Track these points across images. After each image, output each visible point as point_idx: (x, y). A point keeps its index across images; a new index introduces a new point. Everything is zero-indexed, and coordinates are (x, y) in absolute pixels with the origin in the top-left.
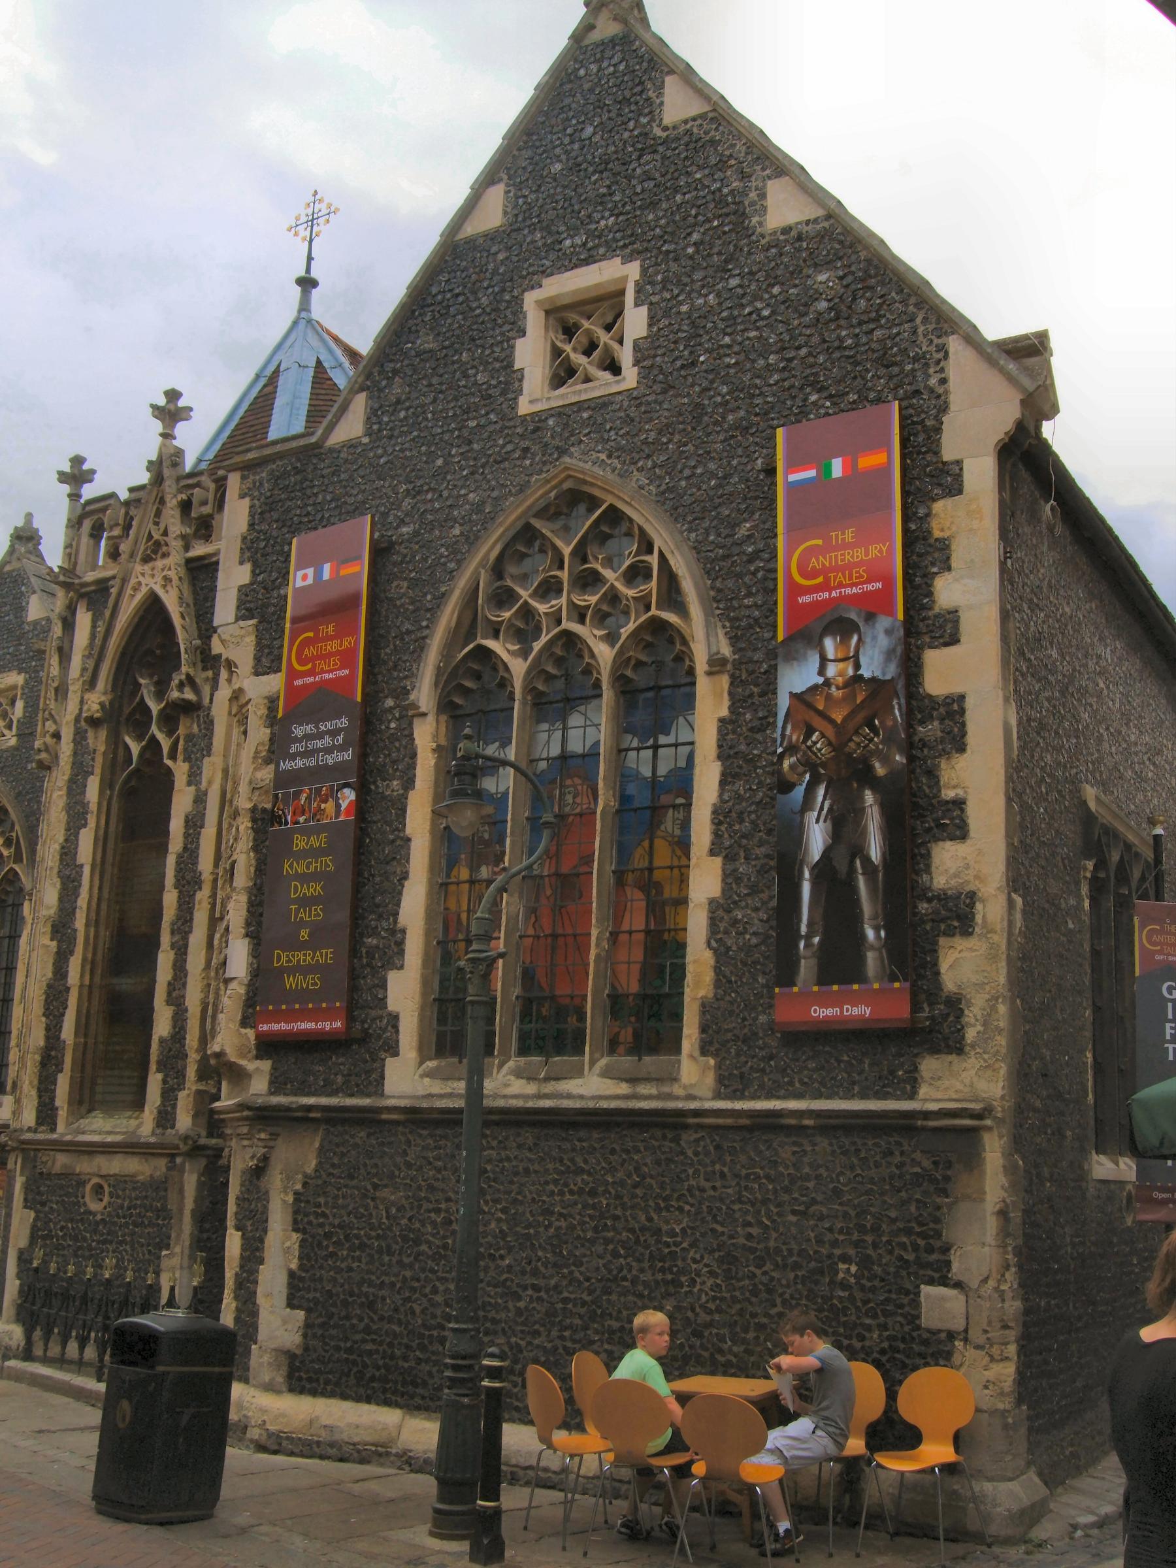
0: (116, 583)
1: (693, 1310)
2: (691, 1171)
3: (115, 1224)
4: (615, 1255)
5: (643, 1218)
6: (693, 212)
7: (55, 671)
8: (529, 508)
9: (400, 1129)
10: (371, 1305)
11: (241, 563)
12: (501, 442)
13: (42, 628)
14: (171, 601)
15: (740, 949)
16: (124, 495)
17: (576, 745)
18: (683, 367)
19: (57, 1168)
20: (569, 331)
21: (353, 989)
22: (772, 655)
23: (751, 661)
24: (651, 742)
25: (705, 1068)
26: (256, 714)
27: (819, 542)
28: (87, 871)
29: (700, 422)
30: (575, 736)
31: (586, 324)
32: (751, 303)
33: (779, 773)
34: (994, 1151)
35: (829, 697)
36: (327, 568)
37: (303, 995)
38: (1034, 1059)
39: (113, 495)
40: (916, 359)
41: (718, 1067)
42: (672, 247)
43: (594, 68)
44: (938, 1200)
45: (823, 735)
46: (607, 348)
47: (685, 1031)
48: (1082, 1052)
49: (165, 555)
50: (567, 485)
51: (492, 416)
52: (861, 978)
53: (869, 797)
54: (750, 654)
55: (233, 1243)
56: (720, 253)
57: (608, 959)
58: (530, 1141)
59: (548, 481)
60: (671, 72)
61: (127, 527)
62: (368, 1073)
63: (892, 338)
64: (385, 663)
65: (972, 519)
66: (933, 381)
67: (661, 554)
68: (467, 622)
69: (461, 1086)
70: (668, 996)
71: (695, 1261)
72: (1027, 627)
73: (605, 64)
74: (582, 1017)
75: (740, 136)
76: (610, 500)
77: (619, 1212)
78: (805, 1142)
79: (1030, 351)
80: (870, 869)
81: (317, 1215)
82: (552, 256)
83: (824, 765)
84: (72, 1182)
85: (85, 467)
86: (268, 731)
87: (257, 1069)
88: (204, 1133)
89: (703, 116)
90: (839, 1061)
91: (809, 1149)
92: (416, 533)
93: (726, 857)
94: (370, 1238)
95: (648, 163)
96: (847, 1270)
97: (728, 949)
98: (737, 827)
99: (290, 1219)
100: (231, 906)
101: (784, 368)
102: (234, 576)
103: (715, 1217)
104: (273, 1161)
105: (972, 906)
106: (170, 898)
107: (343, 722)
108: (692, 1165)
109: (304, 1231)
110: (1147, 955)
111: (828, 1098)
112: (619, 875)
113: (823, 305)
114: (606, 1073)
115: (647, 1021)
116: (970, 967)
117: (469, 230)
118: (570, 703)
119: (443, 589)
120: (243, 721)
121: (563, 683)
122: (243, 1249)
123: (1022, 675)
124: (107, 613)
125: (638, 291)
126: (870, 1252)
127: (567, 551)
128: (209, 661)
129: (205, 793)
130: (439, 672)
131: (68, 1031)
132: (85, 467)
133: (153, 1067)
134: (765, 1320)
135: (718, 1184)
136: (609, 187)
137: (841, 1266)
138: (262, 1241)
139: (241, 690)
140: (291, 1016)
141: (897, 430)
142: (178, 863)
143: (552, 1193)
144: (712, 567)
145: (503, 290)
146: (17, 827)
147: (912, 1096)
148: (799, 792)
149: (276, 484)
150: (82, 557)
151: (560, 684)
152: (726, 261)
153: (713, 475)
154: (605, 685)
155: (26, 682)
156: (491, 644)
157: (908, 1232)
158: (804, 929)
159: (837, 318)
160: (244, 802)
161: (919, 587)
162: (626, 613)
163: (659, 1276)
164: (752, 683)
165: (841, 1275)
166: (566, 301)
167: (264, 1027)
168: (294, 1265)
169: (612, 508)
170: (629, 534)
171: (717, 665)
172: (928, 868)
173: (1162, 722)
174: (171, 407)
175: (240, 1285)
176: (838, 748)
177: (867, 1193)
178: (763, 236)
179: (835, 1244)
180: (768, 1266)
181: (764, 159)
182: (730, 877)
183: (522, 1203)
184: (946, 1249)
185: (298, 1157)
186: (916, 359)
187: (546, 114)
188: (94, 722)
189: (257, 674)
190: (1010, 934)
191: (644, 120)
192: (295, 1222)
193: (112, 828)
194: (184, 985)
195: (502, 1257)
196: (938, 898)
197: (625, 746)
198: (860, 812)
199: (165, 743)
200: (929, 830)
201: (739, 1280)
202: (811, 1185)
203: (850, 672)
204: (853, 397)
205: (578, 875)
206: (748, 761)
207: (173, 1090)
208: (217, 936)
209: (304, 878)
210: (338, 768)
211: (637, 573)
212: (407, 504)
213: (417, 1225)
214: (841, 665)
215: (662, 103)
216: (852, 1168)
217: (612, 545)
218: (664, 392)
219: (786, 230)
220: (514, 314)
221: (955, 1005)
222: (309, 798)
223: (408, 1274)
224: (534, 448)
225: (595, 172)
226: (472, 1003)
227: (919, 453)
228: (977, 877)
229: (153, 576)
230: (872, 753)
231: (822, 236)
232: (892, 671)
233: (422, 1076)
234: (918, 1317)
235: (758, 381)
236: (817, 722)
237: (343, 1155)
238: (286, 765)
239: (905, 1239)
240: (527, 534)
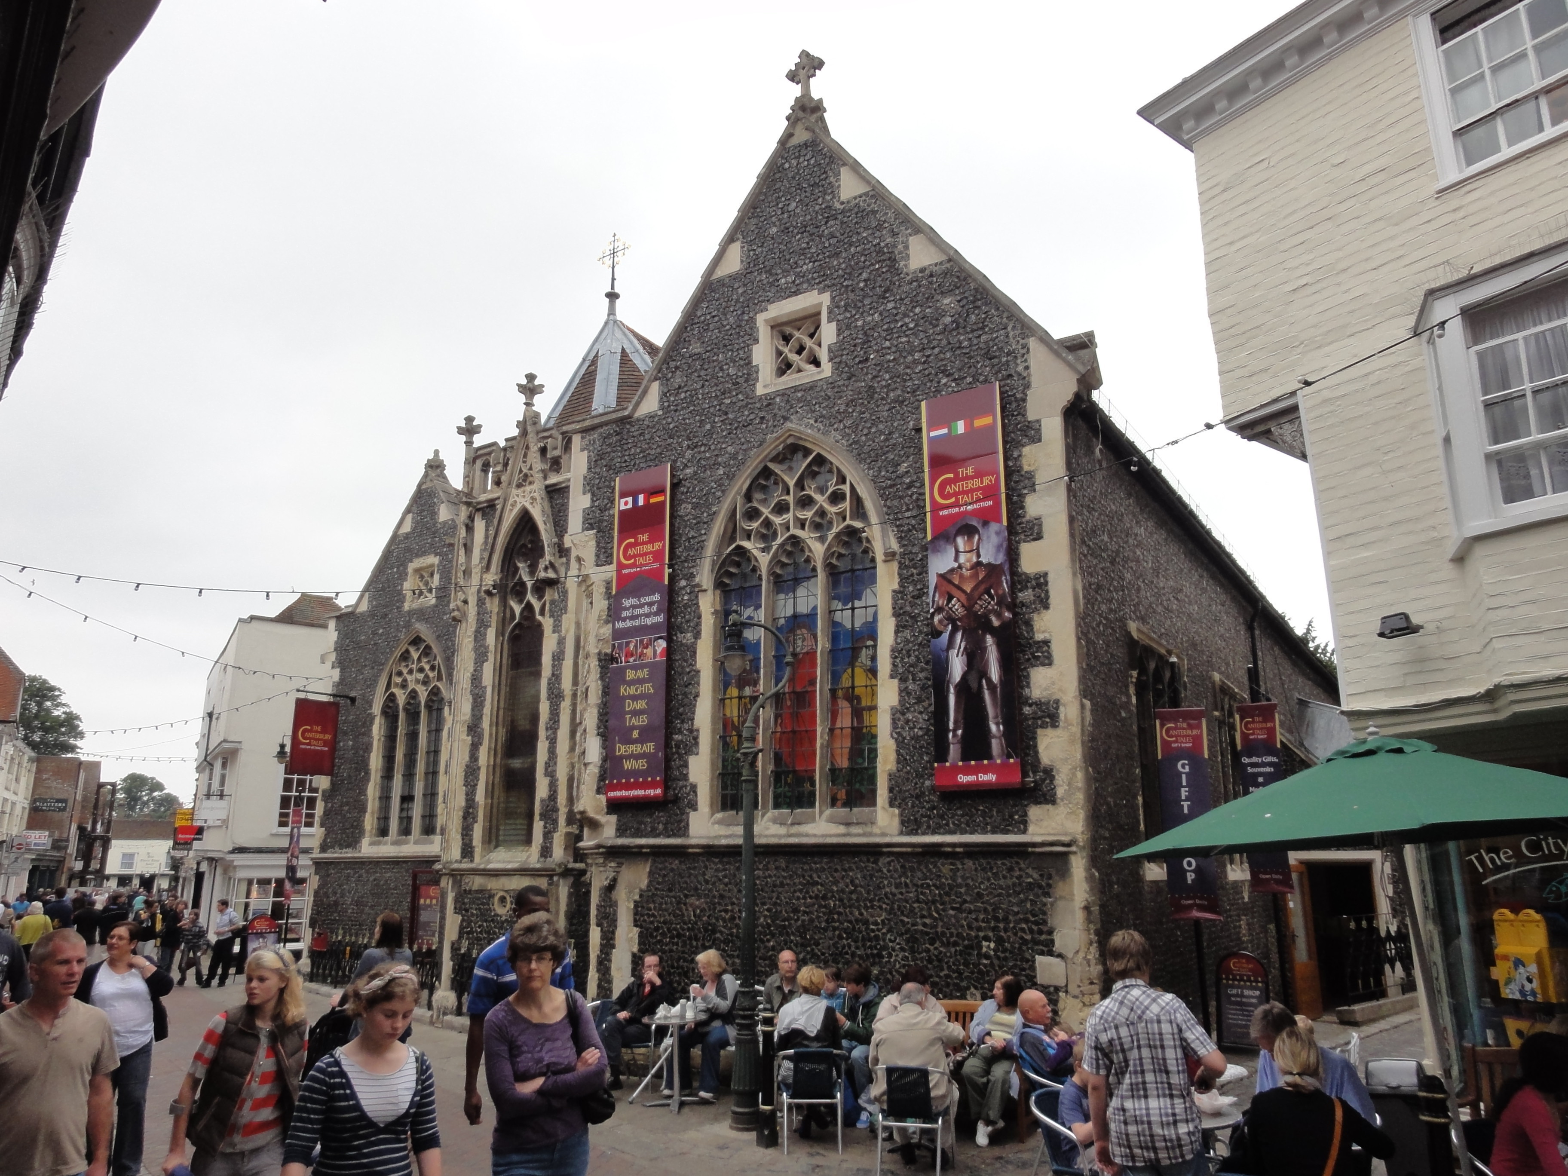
1: (891, 973)
2: (886, 882)
4: (840, 937)
5: (857, 913)
6: (863, 259)
7: (462, 559)
8: (766, 456)
11: (584, 493)
12: (746, 413)
13: (452, 527)
14: (538, 514)
15: (912, 738)
16: (502, 444)
17: (803, 609)
18: (860, 362)
19: (475, 887)
20: (786, 339)
21: (668, 768)
22: (925, 548)
23: (911, 553)
24: (850, 606)
25: (893, 815)
26: (598, 591)
27: (952, 475)
28: (489, 691)
29: (872, 398)
31: (797, 334)
32: (901, 319)
33: (931, 624)
34: (1078, 866)
35: (961, 576)
36: (641, 498)
37: (635, 773)
38: (1102, 805)
39: (495, 444)
40: (1008, 354)
41: (901, 815)
42: (850, 283)
43: (794, 162)
44: (1044, 900)
45: (959, 600)
46: (811, 349)
47: (879, 792)
48: (1135, 797)
49: (530, 483)
50: (789, 441)
51: (740, 397)
52: (990, 757)
53: (989, 640)
54: (910, 548)
55: (595, 935)
56: (880, 286)
57: (829, 745)
58: (783, 865)
59: (778, 438)
60: (844, 164)
61: (506, 465)
62: (680, 821)
63: (993, 340)
64: (679, 557)
65: (1048, 455)
66: (1020, 368)
67: (852, 486)
68: (730, 530)
69: (740, 830)
70: (866, 769)
71: (891, 941)
72: (1087, 524)
73: (801, 160)
74: (813, 784)
75: (890, 207)
76: (817, 450)
77: (841, 910)
78: (958, 863)
79: (1082, 346)
80: (992, 687)
81: (649, 916)
82: (773, 290)
83: (960, 619)
84: (485, 896)
85: (475, 423)
86: (606, 602)
87: (608, 822)
88: (571, 860)
89: (866, 194)
90: (977, 810)
91: (960, 867)
92: (695, 473)
93: (900, 679)
94: (683, 930)
95: (832, 226)
96: (988, 946)
97: (904, 738)
98: (906, 660)
99: (632, 919)
100: (586, 715)
101: (925, 362)
102: (579, 503)
103: (902, 912)
104: (619, 880)
105: (1057, 708)
106: (544, 708)
107: (657, 597)
108: (886, 878)
109: (641, 927)
110: (1165, 743)
111: (971, 833)
112: (833, 692)
113: (948, 320)
114: (831, 820)
115: (854, 787)
116: (1060, 748)
117: (720, 273)
118: (797, 581)
119: (714, 509)
120: (590, 595)
121: (791, 572)
122: (602, 938)
123: (1085, 556)
124: (496, 521)
125: (830, 312)
126: (1002, 934)
127: (791, 483)
128: (563, 551)
129: (564, 638)
130: (714, 563)
132: (475, 423)
133: (537, 817)
134: (937, 979)
135: (904, 890)
136: (808, 243)
137: (985, 943)
138: (613, 933)
139: (587, 576)
140: (628, 787)
141: (998, 402)
142: (549, 684)
143: (798, 898)
144: (887, 492)
145: (743, 313)
146: (438, 658)
147: (1024, 832)
148: (945, 636)
149: (604, 442)
150: (477, 485)
151: (790, 569)
152: (885, 292)
153: (882, 433)
154: (819, 570)
155: (441, 562)
156: (746, 544)
157: (1026, 921)
158: (951, 726)
159: (958, 327)
160: (592, 647)
161: (1016, 502)
162: (830, 523)
163: (869, 951)
164: (912, 568)
165: (984, 950)
166: (784, 320)
167: (612, 794)
169: (819, 455)
170: (830, 471)
171: (890, 556)
172: (1028, 686)
173: (1182, 570)
174: (530, 385)
176: (969, 608)
177: (1000, 895)
178: (908, 274)
179: (979, 929)
180: (937, 944)
181: (907, 221)
182: (904, 692)
183: (780, 905)
184: (1050, 932)
185: (635, 879)
186: (1008, 354)
187: (765, 194)
188: (489, 593)
190: (1083, 726)
191: (828, 198)
192: (635, 921)
193: (505, 661)
194: (555, 763)
195: (768, 941)
196: (1036, 704)
197: (833, 608)
198: (984, 650)
199: (537, 605)
200: (1029, 659)
201: (920, 953)
202: (963, 890)
203: (975, 560)
204: (969, 380)
205: (807, 692)
206: (912, 617)
207: (550, 832)
208: (578, 734)
209: (635, 698)
210: (654, 627)
212: (688, 454)
214: (969, 555)
215: (839, 186)
216: (988, 879)
217: (820, 479)
218: (849, 379)
219: (922, 270)
220: (751, 328)
221: (1049, 773)
222: (636, 646)
224: (768, 417)
225: (798, 233)
226: (745, 781)
227: (1013, 415)
228: (1060, 690)
230: (990, 611)
231: (945, 273)
232: (1000, 559)
233: (713, 824)
234: (1035, 977)
235: (908, 371)
236: (955, 592)
237: (665, 876)
238: (620, 625)
239: (1024, 926)
240: (766, 473)
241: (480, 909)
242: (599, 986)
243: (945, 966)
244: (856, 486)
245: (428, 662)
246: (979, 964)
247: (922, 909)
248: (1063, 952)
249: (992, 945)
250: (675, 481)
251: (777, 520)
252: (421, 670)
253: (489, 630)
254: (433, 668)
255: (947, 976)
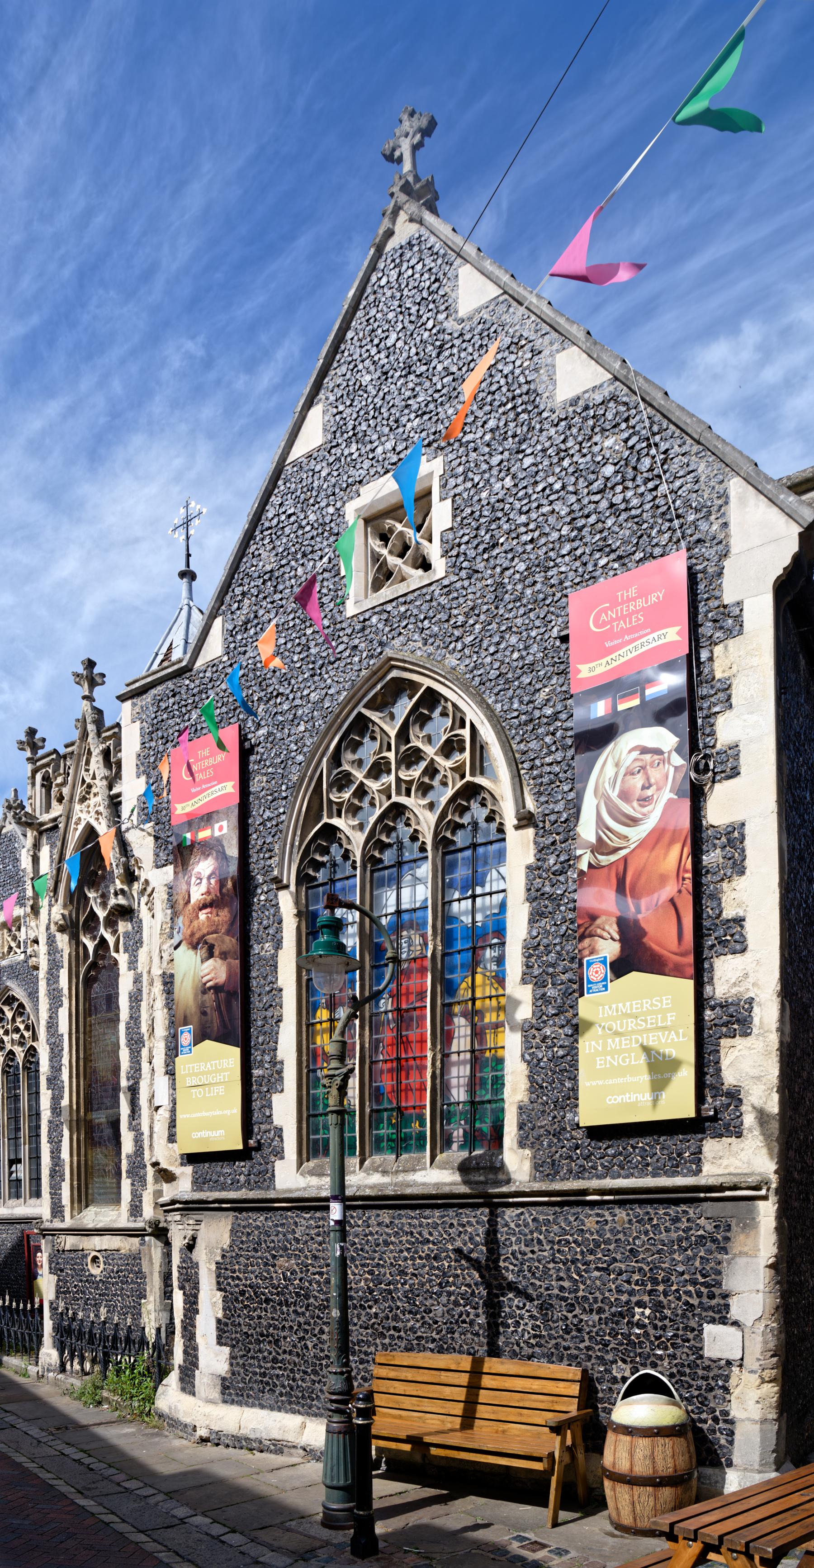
0: (63, 820)
2: (514, 1239)
3: (109, 1283)
9: (289, 1213)
10: (277, 1342)
20: (384, 538)
30: (406, 893)
43: (394, 274)
44: (719, 1256)
49: (95, 795)
56: (514, 436)
71: (518, 1307)
78: (607, 1213)
87: (183, 1173)
91: (610, 1219)
92: (270, 734)
99: (214, 1282)
103: (534, 1274)
104: (199, 1241)
105: (751, 1010)
106: (124, 1055)
108: (514, 1234)
122: (185, 1302)
126: (662, 1298)
127: (393, 733)
131: (65, 1155)
133: (124, 1175)
134: (576, 1352)
135: (536, 1249)
137: (637, 1310)
138: (196, 1296)
142: (127, 1028)
143: (406, 1259)
146: (31, 1017)
156: (336, 821)
157: (694, 1283)
165: (637, 1317)
168: (220, 1315)
175: (184, 1328)
180: (578, 1311)
183: (383, 1266)
185: (215, 1235)
189: (157, 867)
192: (218, 1283)
195: (370, 1307)
199: (111, 939)
211: (450, 747)
213: (307, 1284)
216: (646, 1233)
219: (574, 402)
223: (302, 1320)
229: (89, 812)
234: (701, 1349)
237: (249, 1234)
239: (691, 1288)
241: (74, 1269)
242: (185, 1352)
243: (586, 1337)
244: (478, 725)
245: (23, 1022)
246: (630, 1334)
247: (559, 1270)
248: (741, 1319)
249: (648, 1312)
250: (247, 745)
251: (373, 785)
252: (17, 1030)
253: (62, 971)
254: (27, 1028)
255: (588, 1348)
